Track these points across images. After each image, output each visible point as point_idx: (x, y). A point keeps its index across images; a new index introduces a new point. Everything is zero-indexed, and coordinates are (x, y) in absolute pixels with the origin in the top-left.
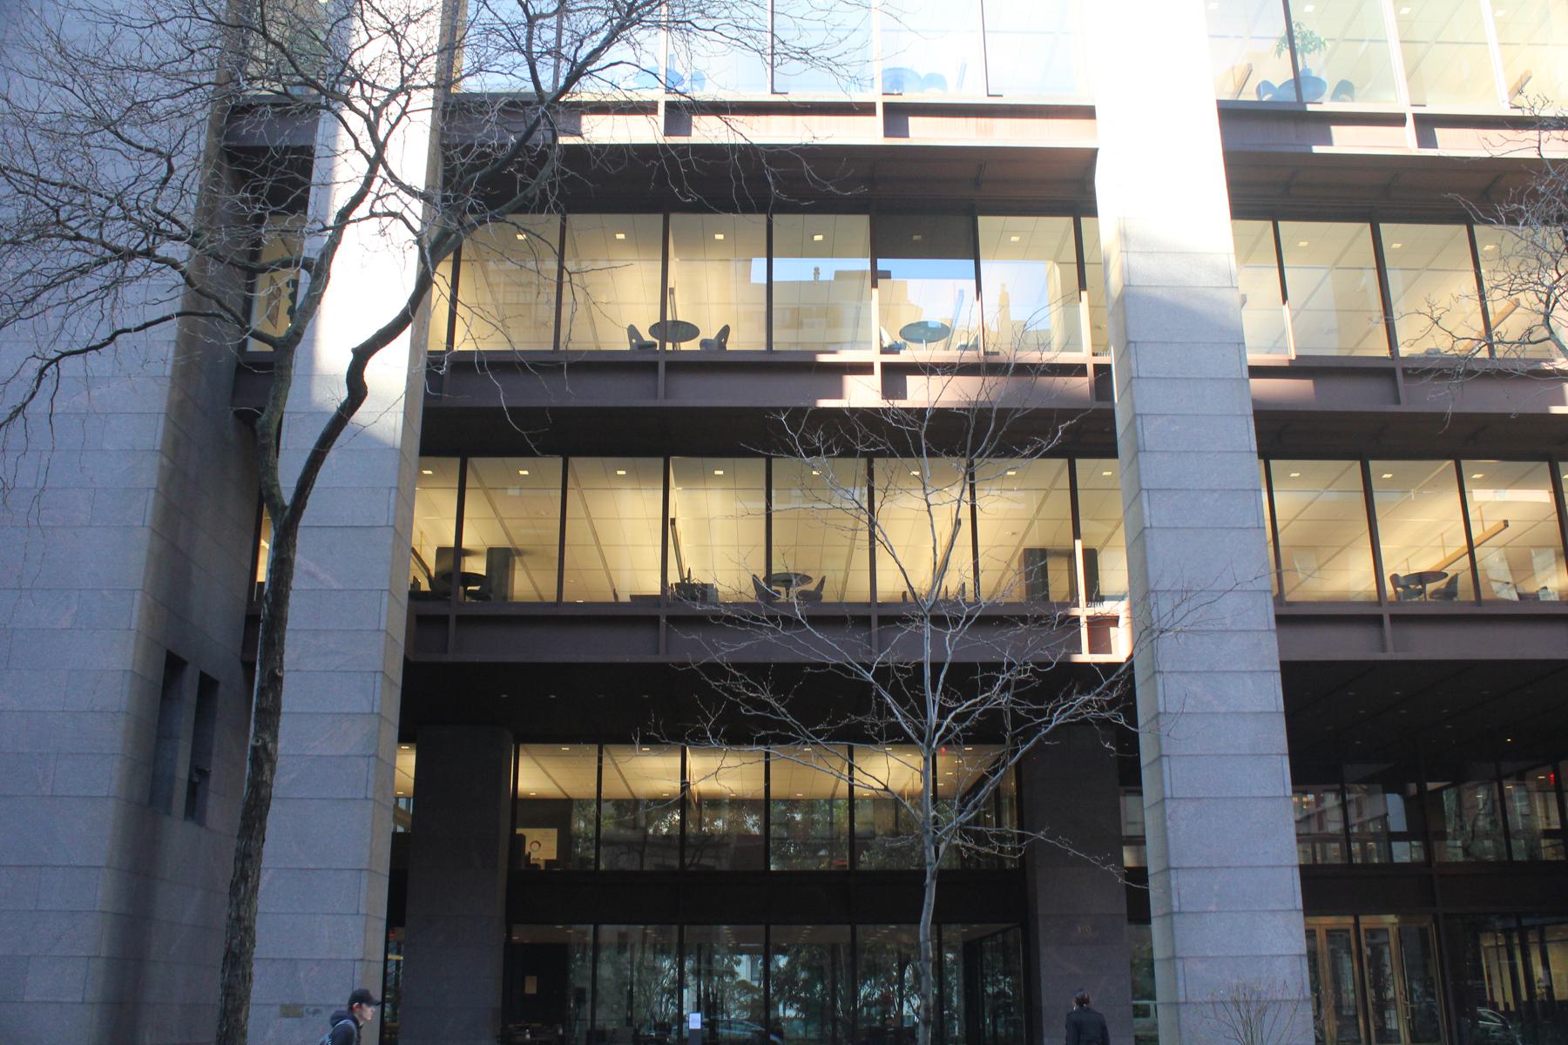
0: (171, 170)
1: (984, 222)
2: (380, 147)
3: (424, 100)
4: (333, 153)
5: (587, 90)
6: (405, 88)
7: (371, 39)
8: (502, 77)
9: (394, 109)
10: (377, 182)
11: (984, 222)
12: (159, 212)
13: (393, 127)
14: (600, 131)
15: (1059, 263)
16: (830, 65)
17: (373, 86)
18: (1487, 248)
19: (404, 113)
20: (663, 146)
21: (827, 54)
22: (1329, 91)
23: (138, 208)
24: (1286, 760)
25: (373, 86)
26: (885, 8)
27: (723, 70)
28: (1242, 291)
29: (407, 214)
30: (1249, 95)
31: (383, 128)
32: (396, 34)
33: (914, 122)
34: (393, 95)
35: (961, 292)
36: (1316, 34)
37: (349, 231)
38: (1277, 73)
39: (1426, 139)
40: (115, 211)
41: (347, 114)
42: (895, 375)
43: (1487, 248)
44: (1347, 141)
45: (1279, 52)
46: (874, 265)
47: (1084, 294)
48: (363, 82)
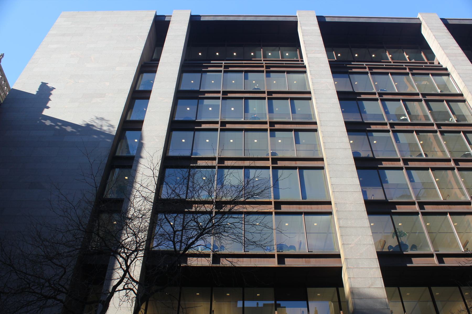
0: (65, 272)
1: (309, 290)
2: (128, 267)
3: (141, 254)
4: (113, 269)
5: (190, 251)
6: (137, 250)
7: (128, 237)
8: (166, 246)
9: (133, 256)
10: (125, 280)
11: (309, 290)
12: (60, 285)
13: (132, 261)
14: (193, 262)
15: (333, 302)
16: (261, 246)
17: (128, 249)
18: (466, 294)
19: (136, 257)
20: (211, 267)
21: (262, 243)
22: (409, 248)
23: (54, 284)
24: (382, 279)
25: (128, 249)
26: (277, 229)
27: (230, 246)
28: (391, 310)
29: (134, 289)
30: (386, 250)
31: (129, 261)
32: (136, 234)
33: (282, 206)
34: (133, 252)
35: (303, 312)
36: (403, 231)
37: (116, 294)
38: (393, 242)
39: (441, 261)
40: (47, 284)
41: (119, 257)
43: (466, 294)
44: (417, 262)
45: (393, 237)
46: (275, 302)
47: (341, 312)
48: (124, 248)
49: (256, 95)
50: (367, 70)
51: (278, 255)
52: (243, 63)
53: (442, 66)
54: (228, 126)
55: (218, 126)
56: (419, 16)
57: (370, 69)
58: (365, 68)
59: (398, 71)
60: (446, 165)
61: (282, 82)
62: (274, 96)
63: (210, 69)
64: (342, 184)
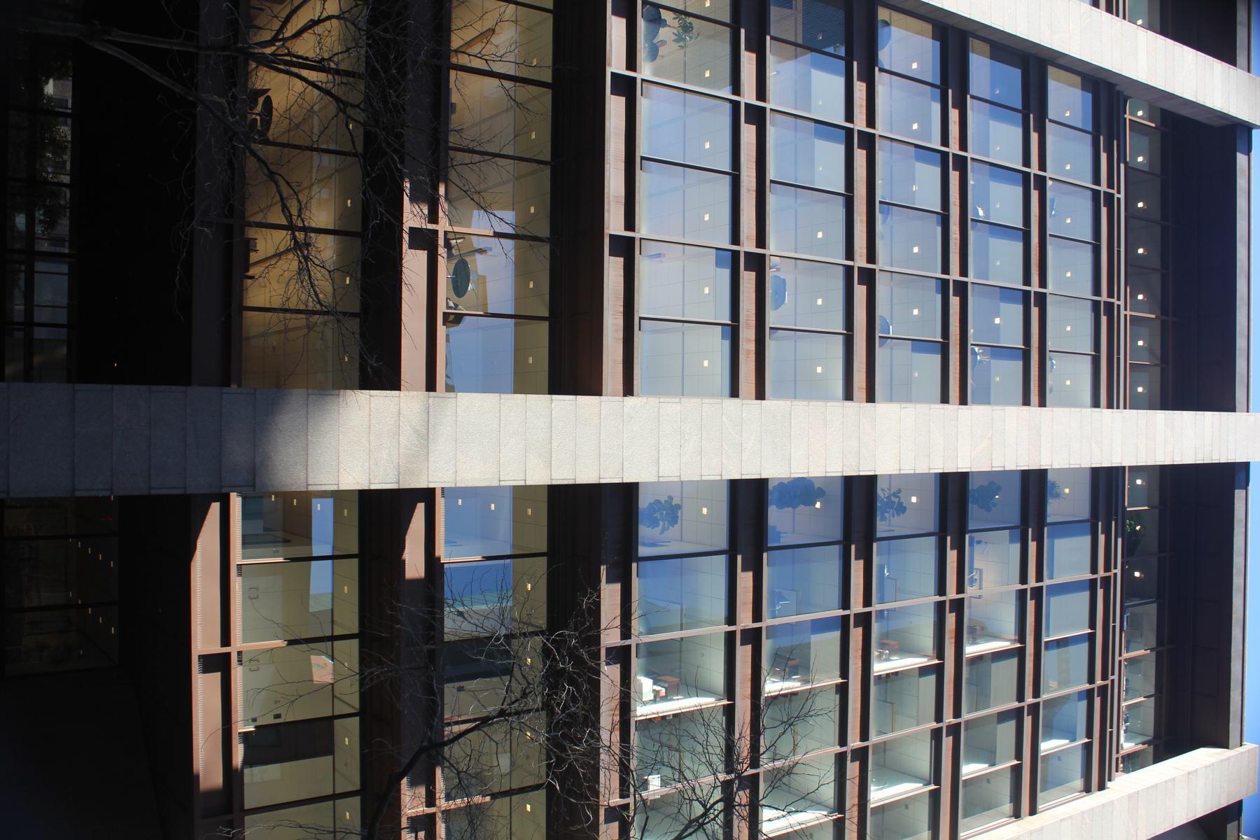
42: (425, 240)
49: (1035, 263)
50: (1099, 682)
51: (630, 646)
52: (1119, 246)
53: (1110, 780)
54: (955, 302)
55: (954, 275)
56: (1248, 746)
57: (1106, 581)
58: (1104, 677)
59: (1102, 311)
60: (854, 710)
61: (1070, 328)
62: (1035, 311)
63: (1104, 157)
64: (809, 438)
